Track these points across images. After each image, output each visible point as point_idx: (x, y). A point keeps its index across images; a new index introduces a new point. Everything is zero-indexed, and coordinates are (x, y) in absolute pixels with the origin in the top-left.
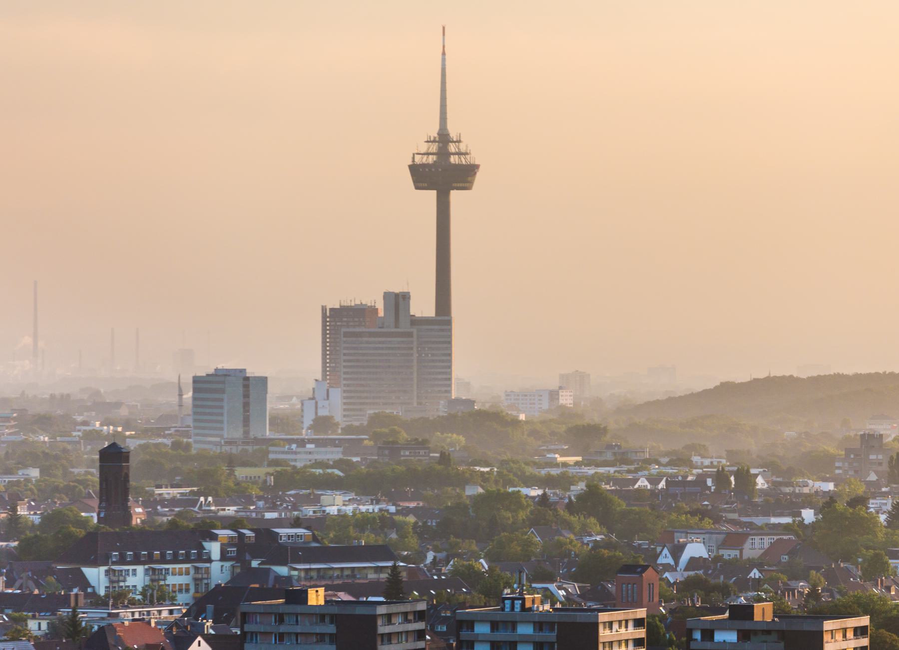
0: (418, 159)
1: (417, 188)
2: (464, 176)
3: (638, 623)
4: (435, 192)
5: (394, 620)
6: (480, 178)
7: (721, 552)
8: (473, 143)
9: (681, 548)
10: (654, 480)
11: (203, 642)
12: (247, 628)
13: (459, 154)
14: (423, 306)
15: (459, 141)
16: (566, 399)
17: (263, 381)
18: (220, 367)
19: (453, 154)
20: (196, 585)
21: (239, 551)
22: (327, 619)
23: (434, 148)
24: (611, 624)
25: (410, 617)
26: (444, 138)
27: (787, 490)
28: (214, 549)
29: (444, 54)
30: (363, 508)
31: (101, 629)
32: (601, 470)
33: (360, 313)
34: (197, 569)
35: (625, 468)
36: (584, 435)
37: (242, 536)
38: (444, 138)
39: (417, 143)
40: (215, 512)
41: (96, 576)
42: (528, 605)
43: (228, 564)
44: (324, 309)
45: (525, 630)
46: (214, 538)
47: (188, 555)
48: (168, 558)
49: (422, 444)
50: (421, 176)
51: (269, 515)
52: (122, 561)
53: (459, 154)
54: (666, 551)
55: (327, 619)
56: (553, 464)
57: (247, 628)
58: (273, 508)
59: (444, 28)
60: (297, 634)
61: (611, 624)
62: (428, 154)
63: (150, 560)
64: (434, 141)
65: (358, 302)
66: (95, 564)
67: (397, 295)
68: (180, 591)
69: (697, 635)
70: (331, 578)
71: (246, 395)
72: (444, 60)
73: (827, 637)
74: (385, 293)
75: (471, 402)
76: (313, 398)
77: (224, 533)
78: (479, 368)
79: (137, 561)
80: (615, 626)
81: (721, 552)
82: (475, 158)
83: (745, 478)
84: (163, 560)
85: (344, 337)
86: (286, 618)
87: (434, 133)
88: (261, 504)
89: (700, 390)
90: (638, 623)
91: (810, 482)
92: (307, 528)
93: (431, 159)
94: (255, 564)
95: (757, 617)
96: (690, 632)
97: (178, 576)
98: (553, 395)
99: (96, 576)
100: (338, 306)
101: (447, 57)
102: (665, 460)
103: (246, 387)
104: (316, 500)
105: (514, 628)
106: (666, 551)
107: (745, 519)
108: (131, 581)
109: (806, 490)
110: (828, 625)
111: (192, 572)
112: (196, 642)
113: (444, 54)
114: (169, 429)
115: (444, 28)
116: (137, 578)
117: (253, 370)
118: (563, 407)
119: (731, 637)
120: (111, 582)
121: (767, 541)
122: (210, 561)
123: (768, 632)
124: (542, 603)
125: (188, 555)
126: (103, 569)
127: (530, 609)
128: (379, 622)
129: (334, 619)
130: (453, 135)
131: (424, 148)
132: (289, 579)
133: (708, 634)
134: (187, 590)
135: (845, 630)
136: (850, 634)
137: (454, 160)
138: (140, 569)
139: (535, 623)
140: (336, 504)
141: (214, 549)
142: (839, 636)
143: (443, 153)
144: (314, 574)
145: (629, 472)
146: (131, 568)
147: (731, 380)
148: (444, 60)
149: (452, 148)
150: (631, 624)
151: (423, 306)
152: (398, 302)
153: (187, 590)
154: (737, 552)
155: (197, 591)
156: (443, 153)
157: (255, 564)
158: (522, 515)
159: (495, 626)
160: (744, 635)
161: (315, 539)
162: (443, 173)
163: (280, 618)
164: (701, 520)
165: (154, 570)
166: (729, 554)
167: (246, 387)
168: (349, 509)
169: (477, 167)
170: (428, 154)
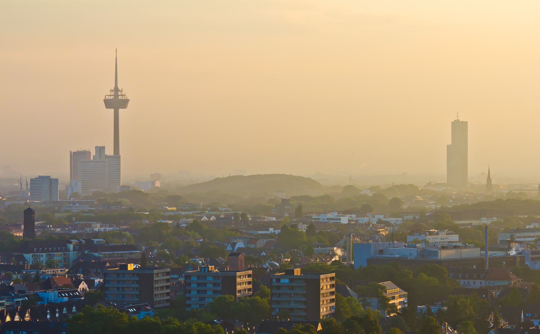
0: (107, 97)
2: (124, 103)
3: (249, 276)
5: (159, 275)
6: (130, 104)
7: (249, 245)
8: (127, 90)
9: (235, 244)
10: (209, 217)
11: (84, 283)
12: (106, 278)
13: (122, 95)
14: (109, 151)
16: (158, 184)
17: (56, 180)
18: (40, 175)
20: (64, 260)
21: (79, 248)
22: (136, 275)
23: (113, 93)
24: (240, 276)
25: (165, 274)
26: (116, 90)
27: (259, 220)
28: (71, 247)
29: (116, 59)
30: (108, 229)
31: (49, 278)
32: (187, 213)
33: (85, 154)
34: (65, 254)
35: (196, 212)
36: (174, 199)
37: (80, 242)
38: (116, 90)
39: (107, 91)
40: (53, 231)
41: (28, 256)
42: (210, 269)
43: (75, 252)
44: (71, 152)
45: (210, 279)
46: (71, 243)
47: (61, 249)
48: (55, 250)
49: (119, 203)
50: (108, 103)
51: (74, 232)
52: (38, 251)
53: (122, 95)
54: (229, 245)
55: (136, 275)
56: (167, 211)
57: (106, 278)
58: (74, 229)
60: (124, 281)
61: (240, 276)
63: (48, 251)
66: (28, 252)
67: (100, 147)
68: (59, 262)
69: (274, 281)
70: (114, 257)
71: (50, 186)
72: (116, 61)
73: (321, 281)
76: (71, 186)
77: (74, 241)
78: (131, 172)
79: (43, 251)
80: (242, 277)
81: (249, 245)
82: (128, 96)
83: (244, 216)
84: (53, 251)
85: (532, 255)
86: (120, 275)
87: (113, 88)
88: (70, 227)
90: (249, 276)
91: (266, 217)
92: (104, 239)
93: (112, 97)
94: (86, 252)
95: (295, 274)
96: (272, 279)
97: (58, 257)
98: (153, 183)
99: (28, 256)
102: (209, 209)
103: (51, 182)
104: (90, 226)
105: (206, 278)
106: (229, 245)
107: (249, 232)
108: (42, 259)
109: (266, 220)
110: (322, 276)
111: (63, 255)
112: (82, 283)
113: (116, 59)
114: (18, 197)
116: (43, 258)
117: (53, 177)
118: (157, 187)
119: (286, 281)
120: (34, 259)
121: (265, 241)
122: (69, 251)
123: (300, 279)
124: (215, 269)
125: (61, 249)
126: (31, 254)
127: (211, 271)
128: (155, 276)
129: (138, 275)
130: (120, 88)
131: (109, 93)
132: (99, 257)
133: (278, 280)
134: (61, 262)
135: (327, 278)
136: (329, 280)
137: (120, 97)
138: (44, 254)
139: (213, 276)
140: (97, 227)
141: (71, 247)
142: (325, 281)
143: (116, 95)
144: (107, 256)
145: (198, 214)
146: (41, 254)
147: (219, 177)
148: (116, 61)
149: (119, 93)
150: (247, 276)
151: (109, 151)
152: (100, 150)
153: (61, 262)
154: (254, 246)
155: (65, 262)
156: (116, 95)
157: (86, 252)
158: (169, 231)
159: (198, 277)
160: (291, 280)
161: (107, 242)
162: (116, 102)
163: (118, 275)
164: (236, 233)
165: (49, 255)
166: (252, 246)
167: (51, 182)
168: (102, 229)
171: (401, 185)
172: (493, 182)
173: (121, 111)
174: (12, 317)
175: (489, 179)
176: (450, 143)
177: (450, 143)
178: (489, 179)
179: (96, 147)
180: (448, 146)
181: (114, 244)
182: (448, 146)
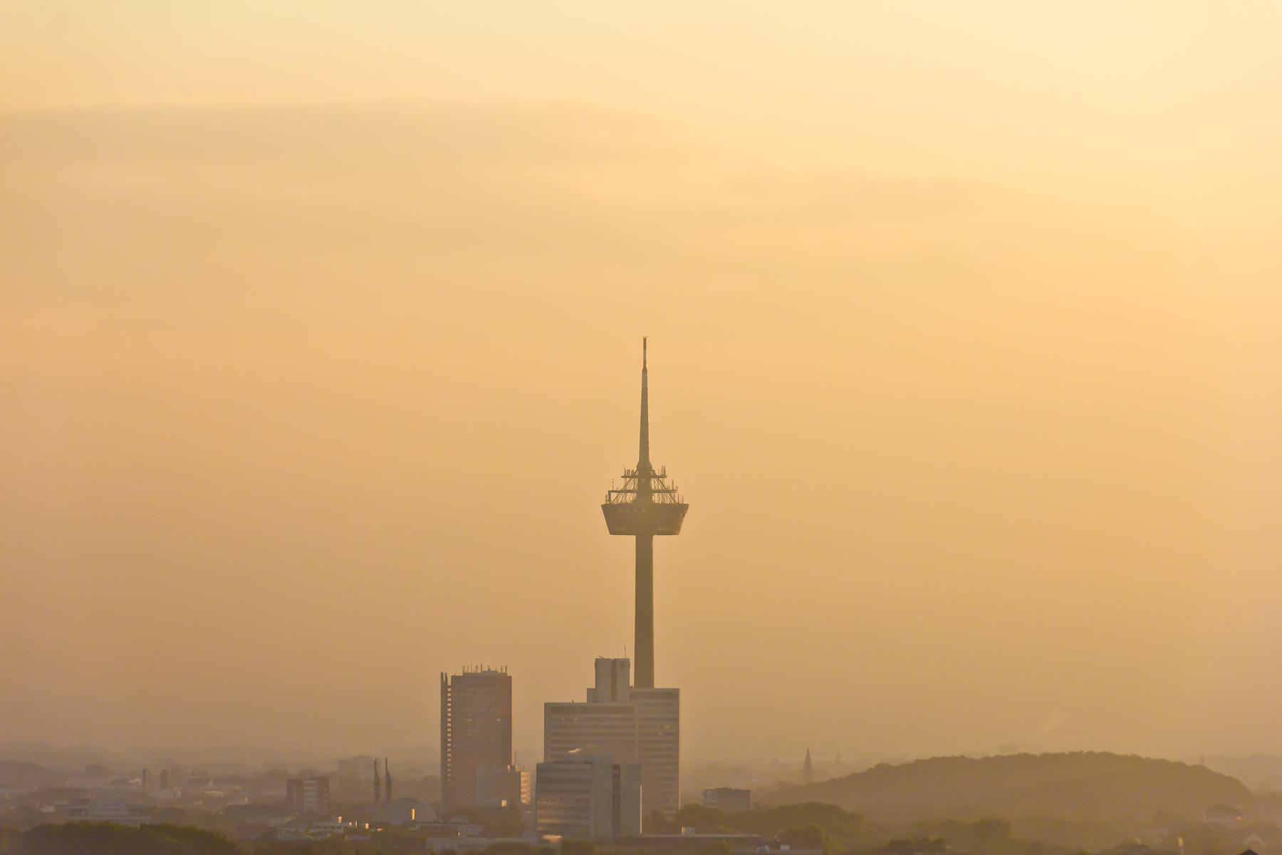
2: (671, 519)
6: (687, 522)
8: (679, 473)
13: (665, 491)
15: (663, 476)
19: (658, 491)
26: (644, 472)
29: (645, 371)
38: (644, 472)
39: (610, 474)
50: (617, 518)
62: (625, 491)
64: (633, 476)
65: (485, 669)
74: (677, 690)
75: (745, 794)
82: (683, 496)
89: (864, 770)
93: (630, 498)
100: (460, 674)
113: (645, 371)
130: (657, 468)
131: (620, 484)
137: (656, 498)
143: (644, 491)
149: (654, 484)
156: (644, 491)
162: (644, 513)
169: (687, 506)
170: (625, 491)
171: (1072, 754)
173: (659, 541)
176: (593, 686)
177: (593, 686)
179: (599, 663)
180: (589, 690)
182: (589, 690)
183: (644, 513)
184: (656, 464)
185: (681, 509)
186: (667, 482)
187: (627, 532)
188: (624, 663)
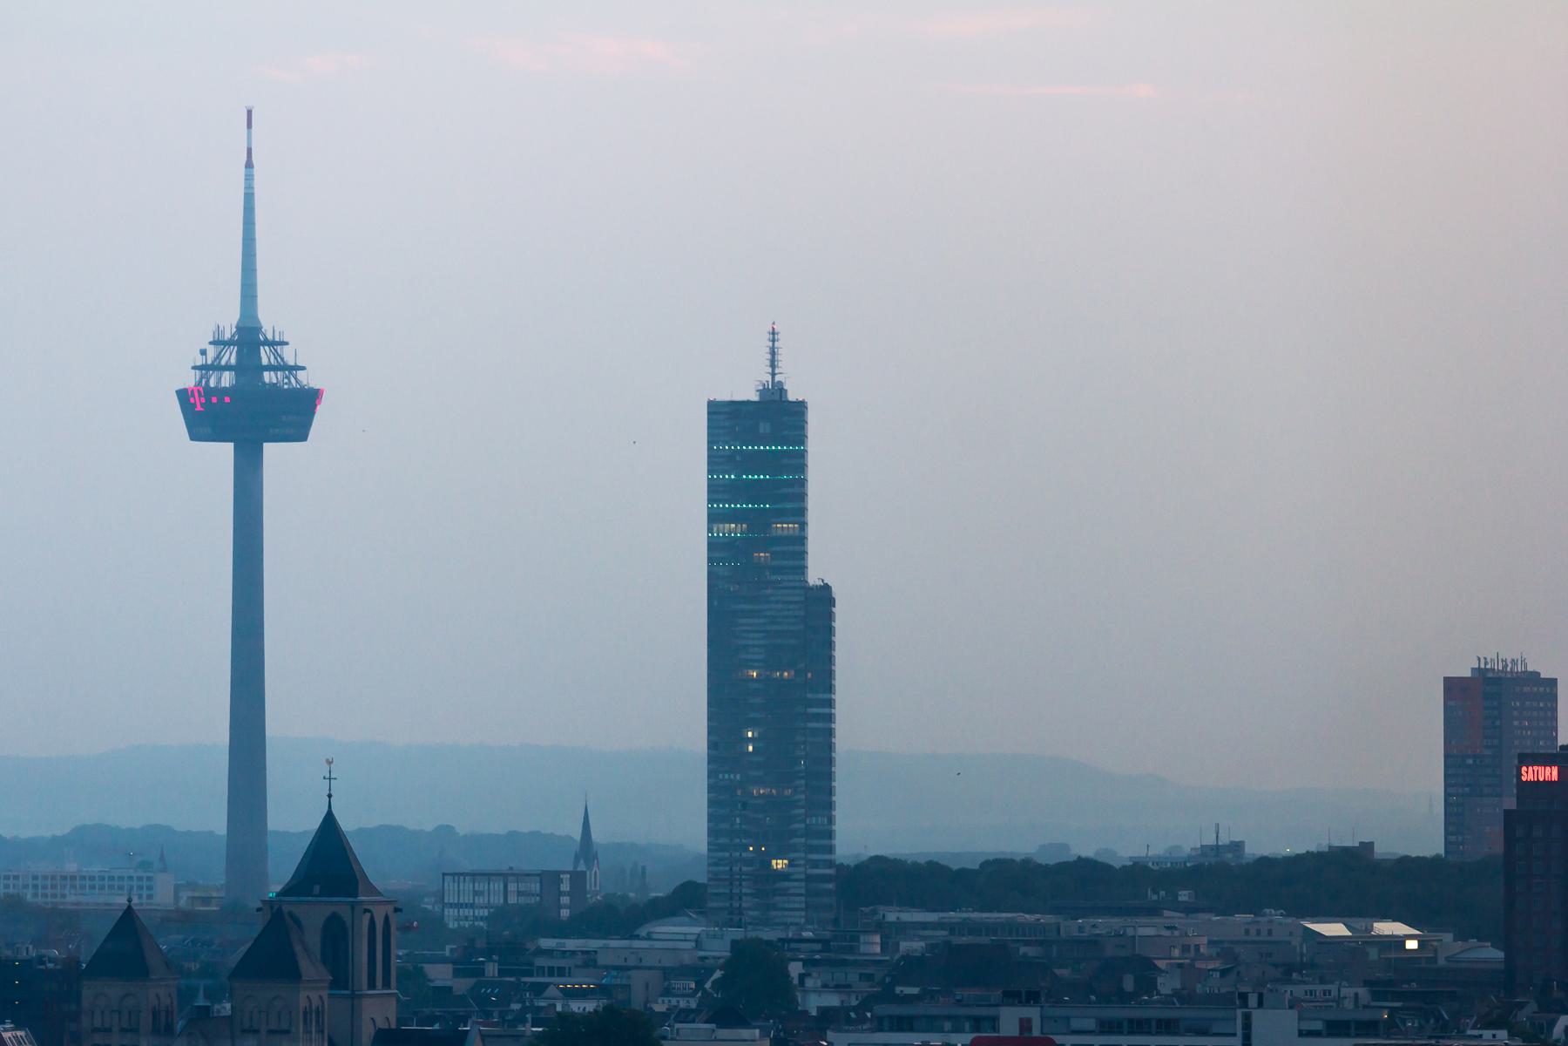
1: (194, 436)
4: (230, 446)
8: (311, 347)
13: (283, 367)
23: (230, 356)
26: (248, 338)
29: (249, 198)
38: (248, 338)
39: (181, 348)
50: (206, 414)
59: (249, 113)
72: (249, 178)
87: (229, 321)
93: (227, 379)
101: (257, 170)
113: (249, 198)
115: (249, 113)
137: (268, 377)
143: (248, 366)
148: (249, 178)
149: (265, 356)
156: (248, 366)
162: (250, 404)
169: (309, 399)
172: (597, 836)
173: (272, 451)
174: (752, 740)
175: (769, 632)
178: (769, 632)
181: (244, 949)
183: (250, 404)
184: (269, 321)
185: (309, 399)
186: (288, 356)
187: (218, 436)
188: (995, 1029)
